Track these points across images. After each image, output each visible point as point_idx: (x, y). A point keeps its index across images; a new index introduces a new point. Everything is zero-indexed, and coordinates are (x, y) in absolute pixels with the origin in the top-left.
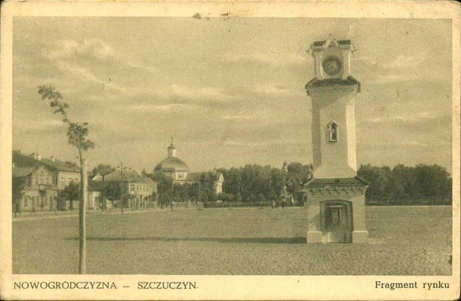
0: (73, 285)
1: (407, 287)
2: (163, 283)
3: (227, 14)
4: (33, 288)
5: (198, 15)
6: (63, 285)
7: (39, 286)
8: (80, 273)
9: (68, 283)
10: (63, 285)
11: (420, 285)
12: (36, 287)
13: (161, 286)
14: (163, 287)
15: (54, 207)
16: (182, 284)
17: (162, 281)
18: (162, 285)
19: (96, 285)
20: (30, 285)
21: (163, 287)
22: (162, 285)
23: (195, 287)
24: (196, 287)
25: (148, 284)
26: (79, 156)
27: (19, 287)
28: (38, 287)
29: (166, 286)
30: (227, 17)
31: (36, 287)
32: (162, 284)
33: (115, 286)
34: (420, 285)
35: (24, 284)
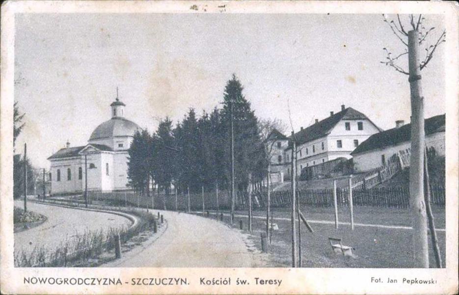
0: (81, 281)
1: (263, 284)
2: (156, 279)
3: (224, 6)
4: (41, 282)
5: (196, 7)
6: (70, 281)
7: (68, 282)
8: (439, 267)
9: (75, 279)
10: (70, 281)
11: (234, 282)
12: (45, 282)
13: (154, 282)
14: (156, 283)
15: (230, 211)
16: (174, 280)
17: (154, 278)
18: (154, 281)
19: (103, 281)
20: (38, 280)
21: (156, 283)
22: (154, 281)
23: (185, 283)
24: (187, 283)
25: (141, 280)
26: (316, 153)
27: (29, 282)
28: (117, 280)
29: (158, 282)
30: (223, 9)
31: (45, 282)
32: (154, 280)
33: (120, 282)
34: (234, 282)
35: (33, 279)
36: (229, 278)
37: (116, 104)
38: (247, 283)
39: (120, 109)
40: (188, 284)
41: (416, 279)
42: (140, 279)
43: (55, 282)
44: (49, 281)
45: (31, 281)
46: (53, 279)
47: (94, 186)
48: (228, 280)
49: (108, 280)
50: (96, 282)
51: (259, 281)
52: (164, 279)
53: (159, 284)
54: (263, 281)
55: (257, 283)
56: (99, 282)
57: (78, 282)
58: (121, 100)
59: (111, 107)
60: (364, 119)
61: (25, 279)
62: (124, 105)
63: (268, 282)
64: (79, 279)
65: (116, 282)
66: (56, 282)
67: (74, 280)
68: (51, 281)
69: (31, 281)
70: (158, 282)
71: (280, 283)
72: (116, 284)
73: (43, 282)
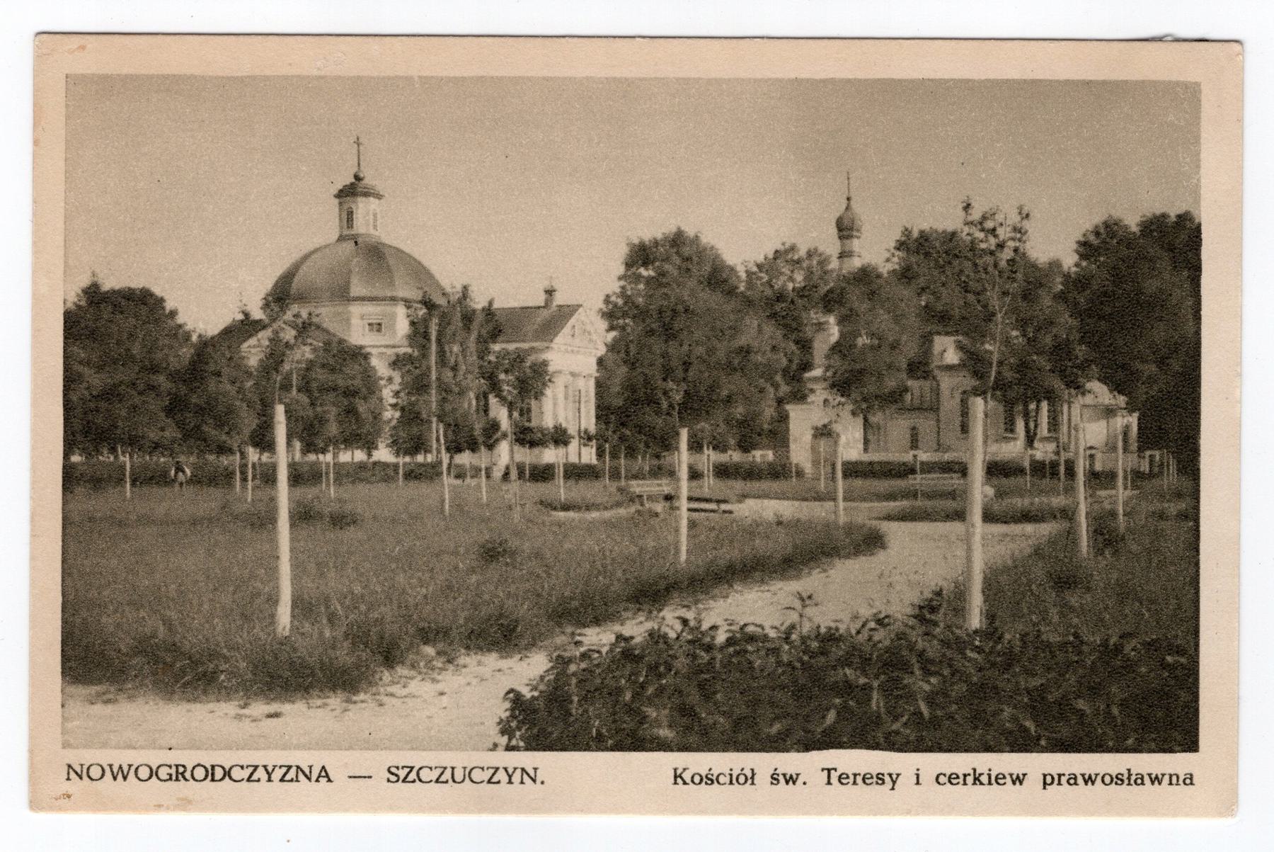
4: (115, 778)
11: (763, 777)
12: (125, 778)
19: (278, 774)
22: (448, 772)
24: (538, 781)
25: (133, 769)
28: (1096, 782)
31: (125, 778)
33: (327, 776)
35: (99, 776)
36: (752, 770)
37: (351, 192)
38: (800, 782)
39: (364, 208)
40: (542, 783)
41: (975, 770)
42: (412, 768)
43: (154, 777)
44: (89, 777)
45: (88, 773)
46: (98, 765)
47: (1138, 219)
48: (749, 775)
49: (293, 770)
50: (260, 773)
51: (834, 775)
52: (720, 774)
53: (463, 781)
54: (848, 777)
55: (829, 783)
56: (269, 774)
57: (213, 774)
58: (369, 180)
59: (337, 201)
60: (334, 454)
61: (69, 766)
62: (379, 196)
63: (859, 779)
64: (213, 767)
65: (314, 777)
66: (157, 775)
67: (140, 776)
68: (144, 773)
69: (88, 773)
70: (458, 777)
71: (894, 782)
72: (317, 781)
73: (120, 777)
